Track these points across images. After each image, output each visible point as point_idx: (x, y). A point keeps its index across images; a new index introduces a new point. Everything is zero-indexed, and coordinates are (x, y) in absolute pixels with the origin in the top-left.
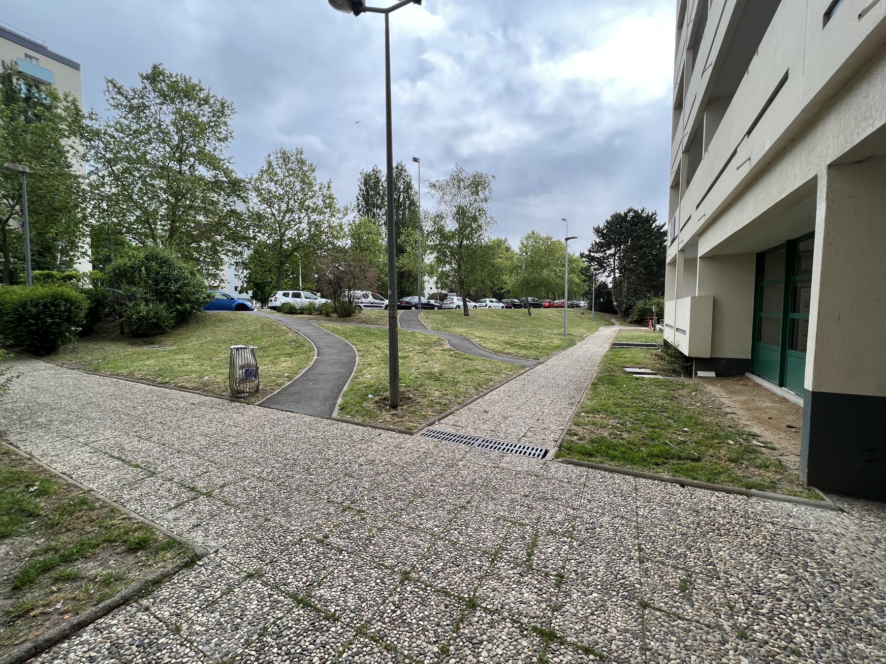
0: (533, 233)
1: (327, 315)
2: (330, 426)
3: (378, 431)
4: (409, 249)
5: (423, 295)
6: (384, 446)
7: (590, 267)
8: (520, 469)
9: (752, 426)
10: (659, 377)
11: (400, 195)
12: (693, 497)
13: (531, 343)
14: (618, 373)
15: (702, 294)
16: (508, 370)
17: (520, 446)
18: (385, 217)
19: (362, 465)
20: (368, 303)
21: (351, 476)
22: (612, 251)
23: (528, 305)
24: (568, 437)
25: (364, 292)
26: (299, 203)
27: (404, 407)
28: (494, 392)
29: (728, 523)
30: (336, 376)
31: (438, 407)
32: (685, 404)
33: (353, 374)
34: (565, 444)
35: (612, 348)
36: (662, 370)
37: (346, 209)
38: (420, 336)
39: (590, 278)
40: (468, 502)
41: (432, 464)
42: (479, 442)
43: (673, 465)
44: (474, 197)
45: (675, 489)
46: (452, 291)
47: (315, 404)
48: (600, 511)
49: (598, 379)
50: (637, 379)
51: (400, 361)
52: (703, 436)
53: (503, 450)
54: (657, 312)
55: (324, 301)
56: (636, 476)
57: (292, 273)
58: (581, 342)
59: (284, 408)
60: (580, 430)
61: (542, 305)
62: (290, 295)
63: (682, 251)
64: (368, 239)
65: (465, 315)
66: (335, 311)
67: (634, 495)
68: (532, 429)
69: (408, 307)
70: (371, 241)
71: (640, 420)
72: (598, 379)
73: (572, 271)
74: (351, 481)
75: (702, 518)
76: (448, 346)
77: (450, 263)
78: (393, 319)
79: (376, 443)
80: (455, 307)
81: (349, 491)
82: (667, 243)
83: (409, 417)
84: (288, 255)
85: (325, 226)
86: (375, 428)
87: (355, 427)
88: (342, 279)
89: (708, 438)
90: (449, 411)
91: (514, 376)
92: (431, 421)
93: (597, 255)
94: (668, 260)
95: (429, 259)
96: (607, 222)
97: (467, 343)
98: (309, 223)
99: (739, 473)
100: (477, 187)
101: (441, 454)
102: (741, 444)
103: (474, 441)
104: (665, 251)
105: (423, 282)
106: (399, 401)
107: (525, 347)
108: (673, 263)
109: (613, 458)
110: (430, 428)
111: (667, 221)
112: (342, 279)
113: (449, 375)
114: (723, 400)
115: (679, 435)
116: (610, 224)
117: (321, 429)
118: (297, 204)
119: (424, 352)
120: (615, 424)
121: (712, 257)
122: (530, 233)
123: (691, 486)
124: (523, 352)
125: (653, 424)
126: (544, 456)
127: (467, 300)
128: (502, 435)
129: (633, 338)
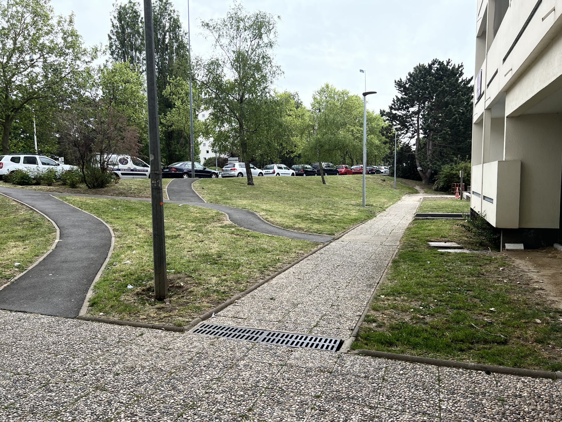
0: (327, 86)
1: (73, 185)
2: (76, 326)
3: (139, 330)
4: (178, 103)
5: (198, 160)
6: (147, 348)
7: (391, 126)
8: (311, 365)
9: (559, 302)
10: (465, 251)
11: (165, 35)
12: (499, 384)
13: (325, 216)
14: (422, 248)
15: (509, 158)
16: (299, 248)
17: (312, 338)
18: (145, 62)
19: (118, 374)
20: (128, 170)
21: (103, 389)
22: (415, 109)
23: (322, 172)
24: (366, 325)
25: (121, 157)
26: (30, 41)
27: (173, 299)
28: (282, 275)
29: (533, 410)
30: (85, 264)
31: (215, 296)
32: (492, 280)
33: (108, 260)
34: (362, 333)
35: (416, 219)
36: (469, 243)
37: (96, 50)
38: (194, 209)
39: (392, 139)
40: (250, 410)
41: (207, 367)
42: (264, 335)
43: (479, 350)
44: (257, 40)
45: (480, 377)
46: (233, 155)
47: (57, 300)
48: (400, 408)
49: (399, 256)
50: (442, 254)
51: (168, 242)
52: (510, 316)
53: (292, 344)
54: (463, 178)
55: (67, 167)
56: (439, 364)
57: (23, 132)
58: (382, 214)
59: (13, 308)
60: (379, 316)
61: (338, 172)
62: (22, 160)
63: (489, 109)
64: (125, 89)
65: (249, 184)
66: (83, 180)
67: (437, 386)
68: (326, 317)
69: (179, 174)
70: (129, 91)
71: (444, 301)
72: (399, 256)
73: (371, 131)
74: (104, 396)
75: (507, 407)
76: (228, 222)
77: (230, 122)
78: (157, 192)
79: (137, 345)
80: (236, 174)
81: (100, 409)
82: (475, 100)
83: (179, 310)
84: (17, 108)
85: (68, 71)
86: (136, 326)
87: (110, 326)
88: (92, 140)
89: (515, 318)
90: (228, 301)
91: (306, 255)
92: (207, 313)
93: (399, 113)
94: (475, 119)
95: (203, 116)
96: (410, 74)
97: (250, 217)
98: (45, 67)
99: (546, 354)
100: (260, 28)
101: (219, 353)
102: (548, 323)
103: (258, 335)
104: (472, 109)
105: (197, 144)
106: (166, 292)
107: (318, 221)
108: (480, 122)
109: (415, 346)
110: (205, 322)
111: (474, 75)
112: (92, 140)
113: (230, 257)
114: (531, 275)
115: (485, 315)
116: (413, 77)
117: (65, 332)
118: (27, 41)
119: (199, 230)
120: (417, 307)
121: (517, 116)
122: (324, 86)
123: (496, 372)
124: (316, 226)
125: (458, 305)
126: (338, 349)
127: (251, 166)
128: (291, 326)
129: (439, 208)
